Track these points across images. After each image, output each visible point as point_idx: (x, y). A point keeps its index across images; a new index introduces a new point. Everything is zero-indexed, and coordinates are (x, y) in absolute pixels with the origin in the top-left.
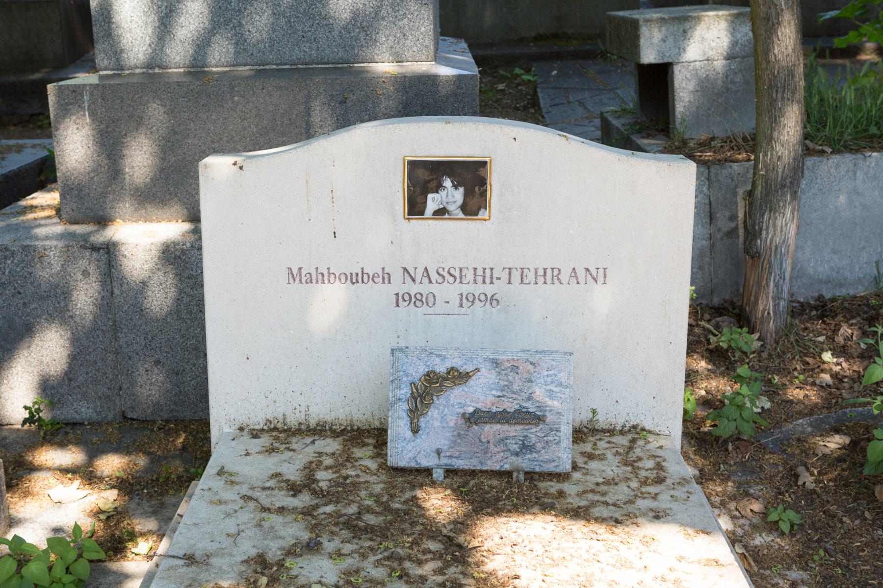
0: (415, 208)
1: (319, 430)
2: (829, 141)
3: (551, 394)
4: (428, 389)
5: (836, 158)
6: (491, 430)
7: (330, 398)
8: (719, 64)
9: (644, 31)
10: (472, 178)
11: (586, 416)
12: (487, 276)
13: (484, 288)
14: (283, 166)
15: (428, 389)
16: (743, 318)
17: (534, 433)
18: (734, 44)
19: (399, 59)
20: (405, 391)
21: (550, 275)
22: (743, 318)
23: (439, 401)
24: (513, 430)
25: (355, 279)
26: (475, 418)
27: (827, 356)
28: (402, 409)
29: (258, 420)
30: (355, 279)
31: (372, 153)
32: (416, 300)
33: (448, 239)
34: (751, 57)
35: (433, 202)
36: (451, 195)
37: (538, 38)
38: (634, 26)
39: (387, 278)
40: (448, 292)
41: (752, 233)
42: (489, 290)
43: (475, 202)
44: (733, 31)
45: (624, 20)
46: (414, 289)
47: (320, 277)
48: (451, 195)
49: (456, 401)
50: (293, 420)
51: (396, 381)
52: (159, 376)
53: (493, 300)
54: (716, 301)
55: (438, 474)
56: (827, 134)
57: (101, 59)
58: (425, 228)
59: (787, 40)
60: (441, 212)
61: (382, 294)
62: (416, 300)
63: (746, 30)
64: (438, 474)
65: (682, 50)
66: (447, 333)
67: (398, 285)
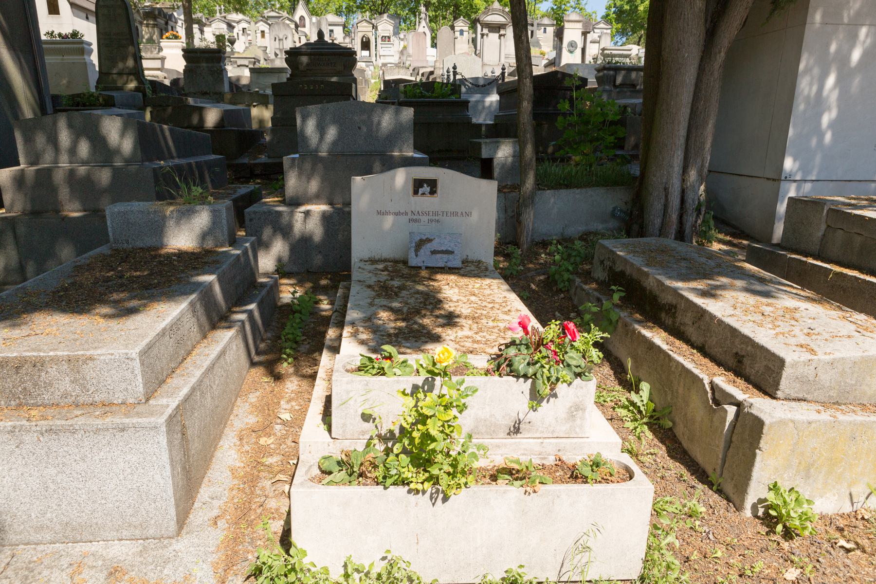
0: (416, 192)
1: (385, 260)
2: (545, 186)
3: (456, 246)
4: (421, 244)
5: (548, 191)
6: (439, 256)
7: (387, 249)
8: (510, 159)
9: (483, 146)
10: (433, 184)
11: (465, 257)
12: (436, 213)
13: (436, 218)
14: (376, 179)
15: (421, 244)
16: (516, 244)
17: (451, 257)
18: (515, 152)
19: (401, 151)
20: (414, 244)
21: (455, 214)
22: (516, 244)
23: (424, 248)
24: (445, 256)
25: (397, 214)
26: (434, 252)
27: (543, 255)
28: (413, 249)
29: (366, 257)
30: (397, 214)
31: (401, 177)
32: (416, 221)
33: (425, 202)
34: (519, 156)
35: (421, 191)
36: (426, 188)
37: (440, 151)
38: (480, 144)
39: (406, 214)
40: (425, 218)
41: (519, 214)
42: (437, 218)
43: (433, 192)
44: (514, 147)
45: (476, 143)
46: (415, 217)
47: (387, 213)
48: (426, 188)
49: (429, 247)
50: (377, 258)
51: (411, 242)
52: (320, 257)
53: (438, 221)
54: (507, 241)
55: (423, 268)
56: (542, 183)
57: (300, 149)
58: (419, 199)
59: (529, 151)
60: (423, 194)
61: (404, 219)
62: (416, 221)
63: (518, 148)
64: (423, 268)
65: (495, 152)
66: (424, 229)
67: (410, 216)
